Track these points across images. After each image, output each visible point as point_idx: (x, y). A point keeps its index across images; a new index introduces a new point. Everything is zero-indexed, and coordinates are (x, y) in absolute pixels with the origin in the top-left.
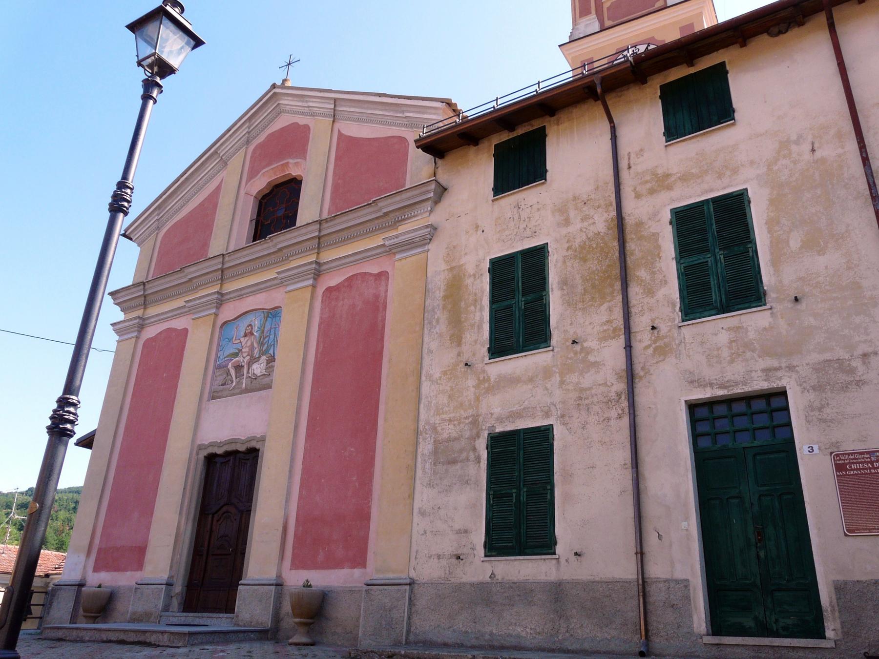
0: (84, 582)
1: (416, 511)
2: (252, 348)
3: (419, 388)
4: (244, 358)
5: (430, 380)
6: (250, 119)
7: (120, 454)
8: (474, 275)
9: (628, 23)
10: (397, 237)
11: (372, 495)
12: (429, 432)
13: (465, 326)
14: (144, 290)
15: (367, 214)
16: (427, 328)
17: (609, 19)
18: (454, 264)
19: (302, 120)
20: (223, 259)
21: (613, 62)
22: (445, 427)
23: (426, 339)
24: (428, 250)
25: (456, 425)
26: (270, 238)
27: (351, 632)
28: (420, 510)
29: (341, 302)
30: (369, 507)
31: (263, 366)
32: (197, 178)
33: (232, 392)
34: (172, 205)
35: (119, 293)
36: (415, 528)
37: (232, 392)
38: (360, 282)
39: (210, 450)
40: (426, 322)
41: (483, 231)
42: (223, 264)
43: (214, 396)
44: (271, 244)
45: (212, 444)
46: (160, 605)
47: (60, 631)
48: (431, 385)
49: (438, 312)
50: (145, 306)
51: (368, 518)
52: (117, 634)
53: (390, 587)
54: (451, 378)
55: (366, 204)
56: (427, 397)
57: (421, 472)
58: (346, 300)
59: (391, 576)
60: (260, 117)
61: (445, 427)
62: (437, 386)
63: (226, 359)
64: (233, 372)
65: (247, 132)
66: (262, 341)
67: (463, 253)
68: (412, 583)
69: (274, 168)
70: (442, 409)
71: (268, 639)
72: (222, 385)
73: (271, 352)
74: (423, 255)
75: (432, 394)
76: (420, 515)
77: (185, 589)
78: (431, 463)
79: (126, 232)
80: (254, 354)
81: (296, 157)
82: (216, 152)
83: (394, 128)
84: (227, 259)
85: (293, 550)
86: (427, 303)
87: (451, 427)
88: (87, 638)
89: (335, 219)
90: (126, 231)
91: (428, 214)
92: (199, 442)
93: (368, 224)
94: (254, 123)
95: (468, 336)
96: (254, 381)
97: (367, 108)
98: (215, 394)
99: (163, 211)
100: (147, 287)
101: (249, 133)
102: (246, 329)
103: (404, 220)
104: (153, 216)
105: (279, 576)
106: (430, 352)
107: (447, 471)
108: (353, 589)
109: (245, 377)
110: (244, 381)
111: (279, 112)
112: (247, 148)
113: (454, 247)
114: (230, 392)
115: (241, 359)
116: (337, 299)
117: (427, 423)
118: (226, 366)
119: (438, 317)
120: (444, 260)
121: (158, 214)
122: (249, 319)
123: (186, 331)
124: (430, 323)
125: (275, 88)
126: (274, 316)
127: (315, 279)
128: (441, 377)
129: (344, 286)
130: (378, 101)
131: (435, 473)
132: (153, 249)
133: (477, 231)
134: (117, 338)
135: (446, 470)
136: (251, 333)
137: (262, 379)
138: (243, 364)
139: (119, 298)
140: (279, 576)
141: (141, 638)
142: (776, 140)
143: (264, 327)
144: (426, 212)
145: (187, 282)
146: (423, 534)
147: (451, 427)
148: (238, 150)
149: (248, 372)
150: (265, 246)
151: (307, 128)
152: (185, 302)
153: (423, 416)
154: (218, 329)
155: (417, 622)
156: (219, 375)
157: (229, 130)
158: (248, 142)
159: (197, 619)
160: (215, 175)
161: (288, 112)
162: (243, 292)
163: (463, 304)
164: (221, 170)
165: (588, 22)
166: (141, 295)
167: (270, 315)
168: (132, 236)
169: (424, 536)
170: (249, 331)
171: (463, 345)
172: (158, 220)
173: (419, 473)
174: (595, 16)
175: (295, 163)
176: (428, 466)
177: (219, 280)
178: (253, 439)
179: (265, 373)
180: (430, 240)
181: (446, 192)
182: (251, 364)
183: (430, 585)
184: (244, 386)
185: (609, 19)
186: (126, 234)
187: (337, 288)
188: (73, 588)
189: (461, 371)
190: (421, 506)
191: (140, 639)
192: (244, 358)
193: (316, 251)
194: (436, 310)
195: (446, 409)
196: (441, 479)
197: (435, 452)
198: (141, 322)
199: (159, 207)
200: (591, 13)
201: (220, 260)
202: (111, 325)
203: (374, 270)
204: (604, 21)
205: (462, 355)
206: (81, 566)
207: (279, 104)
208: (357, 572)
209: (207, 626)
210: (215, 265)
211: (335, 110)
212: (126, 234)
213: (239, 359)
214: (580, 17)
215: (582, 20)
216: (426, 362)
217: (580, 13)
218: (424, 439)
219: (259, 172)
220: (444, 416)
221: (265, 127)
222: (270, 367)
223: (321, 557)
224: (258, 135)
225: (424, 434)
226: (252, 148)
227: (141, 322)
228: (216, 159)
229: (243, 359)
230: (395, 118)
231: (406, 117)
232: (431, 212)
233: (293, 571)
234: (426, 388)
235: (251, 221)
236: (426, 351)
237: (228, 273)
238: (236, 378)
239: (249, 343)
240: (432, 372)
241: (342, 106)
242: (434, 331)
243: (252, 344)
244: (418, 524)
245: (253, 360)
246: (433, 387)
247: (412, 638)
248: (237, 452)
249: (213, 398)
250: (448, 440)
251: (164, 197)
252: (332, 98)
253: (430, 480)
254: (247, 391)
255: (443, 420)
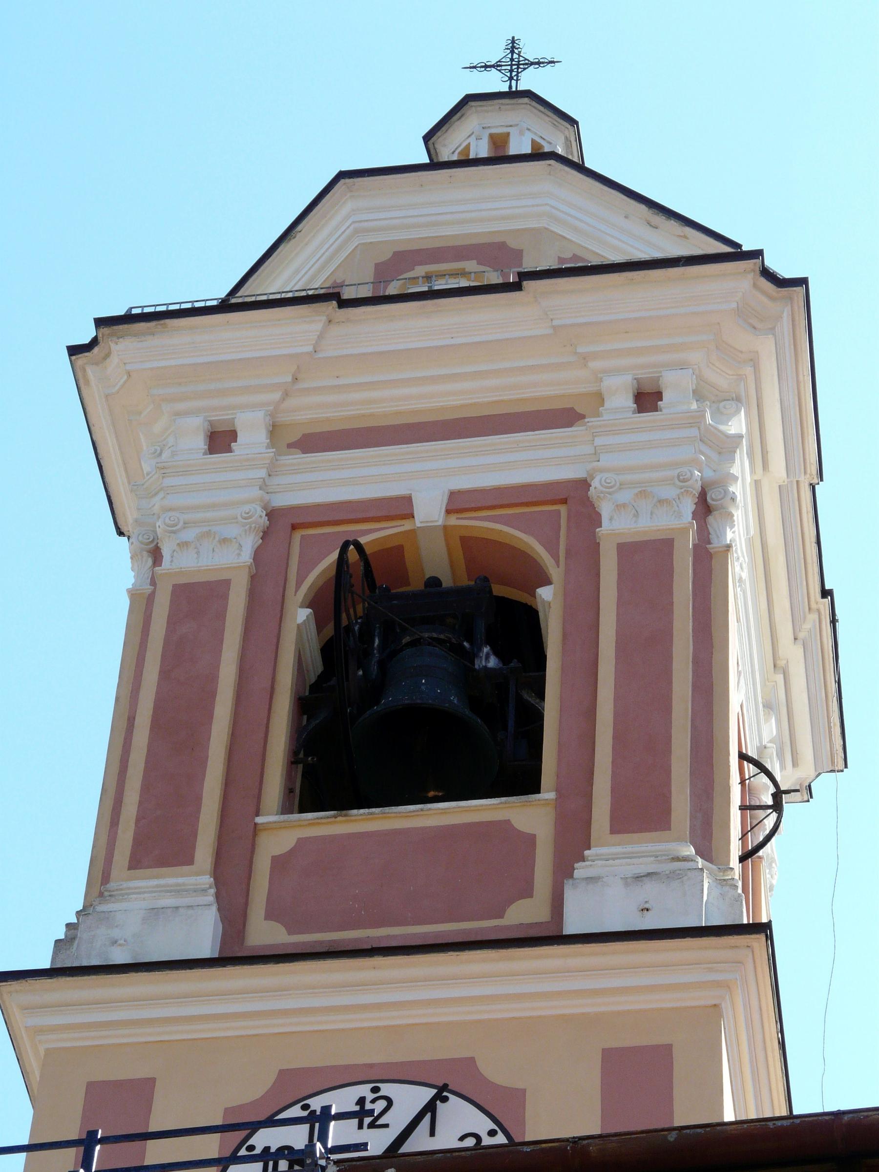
21: (254, 1127)
142: (702, 406)
165: (169, 901)
174: (207, 880)
200: (190, 861)
204: (245, 916)
214: (135, 863)
217: (138, 842)
252: (69, 359)
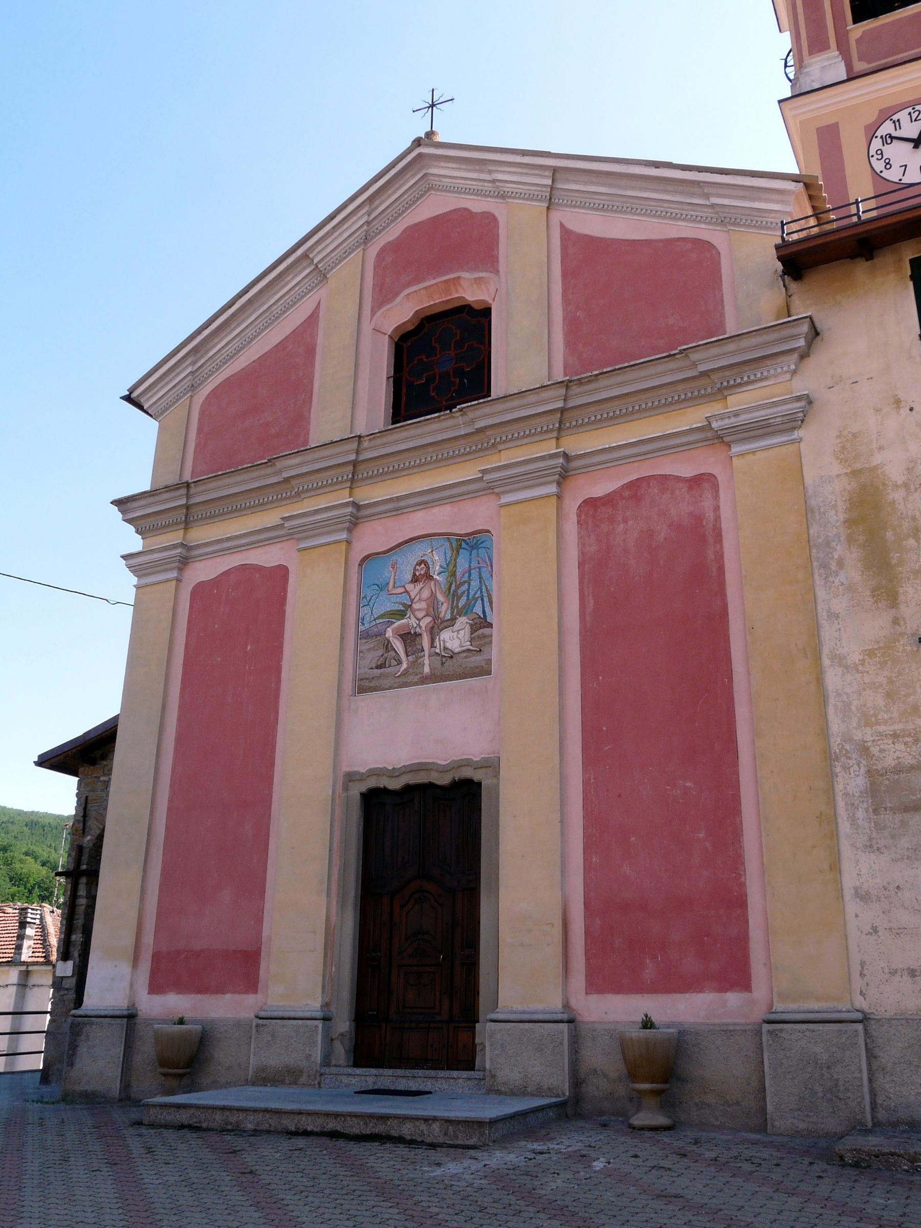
0: (134, 1011)
1: (848, 894)
2: (433, 602)
3: (820, 680)
4: (419, 620)
5: (840, 666)
6: (371, 199)
7: (172, 786)
8: (906, 485)
9: (903, 66)
10: (735, 416)
11: (743, 864)
12: (854, 756)
13: (901, 573)
14: (188, 496)
15: (664, 373)
16: (820, 575)
17: (860, 59)
18: (858, 466)
19: (477, 205)
20: (359, 443)
22: (887, 746)
23: (821, 594)
24: (800, 440)
25: (910, 744)
26: (461, 410)
27: (738, 1103)
28: (856, 892)
29: (622, 525)
30: (742, 885)
31: (465, 634)
32: (268, 300)
33: (403, 679)
34: (219, 346)
35: (136, 500)
36: (852, 924)
37: (403, 679)
38: (656, 491)
39: (372, 783)
40: (815, 564)
41: (911, 409)
42: (358, 452)
43: (363, 687)
44: (460, 420)
45: (375, 773)
46: (317, 1055)
47: (182, 1111)
48: (843, 674)
49: (838, 548)
50: (187, 525)
51: (741, 902)
52: (320, 1121)
53: (820, 1027)
54: (886, 662)
55: (664, 355)
56: (839, 695)
57: (848, 825)
58: (630, 522)
59: (816, 1006)
60: (389, 196)
61: (887, 746)
62: (858, 676)
63: (378, 621)
64: (398, 645)
65: (367, 222)
66: (455, 591)
67: (874, 446)
68: (865, 1019)
69: (430, 286)
70: (876, 715)
71: (567, 1116)
72: (379, 667)
73: (478, 609)
74: (791, 448)
75: (848, 690)
76: (858, 900)
77: (353, 1024)
78: (867, 810)
79: (131, 393)
80: (439, 613)
81: (476, 269)
82: (305, 256)
83: (684, 224)
84: (365, 444)
85: (588, 960)
86: (811, 531)
87: (900, 746)
88: (250, 1126)
89: (598, 379)
90: (132, 391)
91: (788, 376)
92: (346, 768)
93: (664, 391)
94: (378, 207)
95: (911, 591)
96: (449, 662)
97: (627, 188)
98: (366, 683)
99: (202, 356)
100: (192, 491)
101: (368, 223)
102: (415, 569)
103: (740, 385)
104: (184, 365)
105: (567, 1006)
106: (833, 616)
107: (903, 824)
108: (731, 1028)
109: (426, 653)
110: (427, 661)
111: (427, 187)
112: (364, 250)
113: (855, 436)
114: (397, 680)
115: (413, 622)
116: (611, 520)
117: (847, 739)
118: (382, 634)
119: (840, 556)
120: (837, 458)
121: (194, 363)
122: (419, 551)
123: (282, 572)
124: (825, 566)
125: (419, 145)
126: (474, 547)
127: (559, 484)
128: (863, 660)
129: (622, 498)
130: (618, 171)
131: (879, 827)
132: (187, 423)
133: (898, 408)
134: (134, 580)
135: (902, 821)
136: (428, 577)
137: (466, 657)
138: (418, 630)
139: (134, 510)
140: (567, 1006)
141: (380, 1128)
143: (455, 566)
144: (787, 372)
145: (279, 483)
146: (869, 934)
147: (900, 746)
148: (347, 253)
149: (432, 645)
150: (450, 422)
151: (490, 220)
152: (283, 519)
153: (836, 726)
154: (355, 568)
155: (887, 1086)
156: (369, 650)
157: (331, 217)
158: (366, 240)
159: (404, 1081)
160: (303, 297)
161: (447, 190)
162: (403, 503)
163: (889, 535)
164: (313, 288)
165: (826, 63)
166: (182, 505)
167: (464, 545)
168: (142, 400)
169: (874, 937)
170: (422, 572)
171: (902, 607)
172: (192, 373)
173: (844, 827)
174: (837, 53)
175: (476, 279)
176: (860, 814)
177: (346, 481)
178: (467, 763)
179: (471, 648)
180: (802, 421)
181: (819, 338)
182: (436, 630)
183: (903, 1022)
184: (427, 670)
185: (860, 59)
186: (134, 395)
187: (608, 500)
188: (118, 1021)
189: (904, 650)
190: (858, 884)
191: (376, 1130)
192: (419, 620)
193: (555, 434)
194: (834, 544)
195: (883, 716)
196: (893, 837)
197: (873, 790)
198: (184, 552)
199: (195, 350)
200: (829, 48)
201: (354, 445)
202: (123, 557)
203: (687, 471)
205: (902, 623)
206: (126, 983)
207: (425, 175)
208: (733, 999)
209: (430, 1093)
210: (348, 452)
211: (552, 188)
212: (134, 395)
213: (410, 621)
214: (811, 53)
215: (813, 60)
216: (828, 632)
218: (846, 768)
219: (397, 294)
220: (881, 728)
221: (400, 215)
222: (479, 637)
223: (649, 972)
224: (384, 228)
225: (843, 759)
226: (373, 250)
227: (184, 552)
228: (305, 268)
229: (419, 621)
230: (686, 207)
231: (713, 206)
232: (794, 372)
233: (594, 998)
234: (833, 679)
235: (388, 378)
236: (825, 614)
237: (363, 471)
238: (407, 656)
239: (426, 594)
240: (841, 651)
241: (568, 181)
242: (837, 581)
243: (433, 595)
244: (857, 916)
245: (438, 626)
246: (849, 678)
247: (882, 1115)
248: (431, 786)
249: (362, 690)
250: (898, 770)
251: (206, 332)
253: (871, 839)
254: (434, 678)
255: (880, 734)
